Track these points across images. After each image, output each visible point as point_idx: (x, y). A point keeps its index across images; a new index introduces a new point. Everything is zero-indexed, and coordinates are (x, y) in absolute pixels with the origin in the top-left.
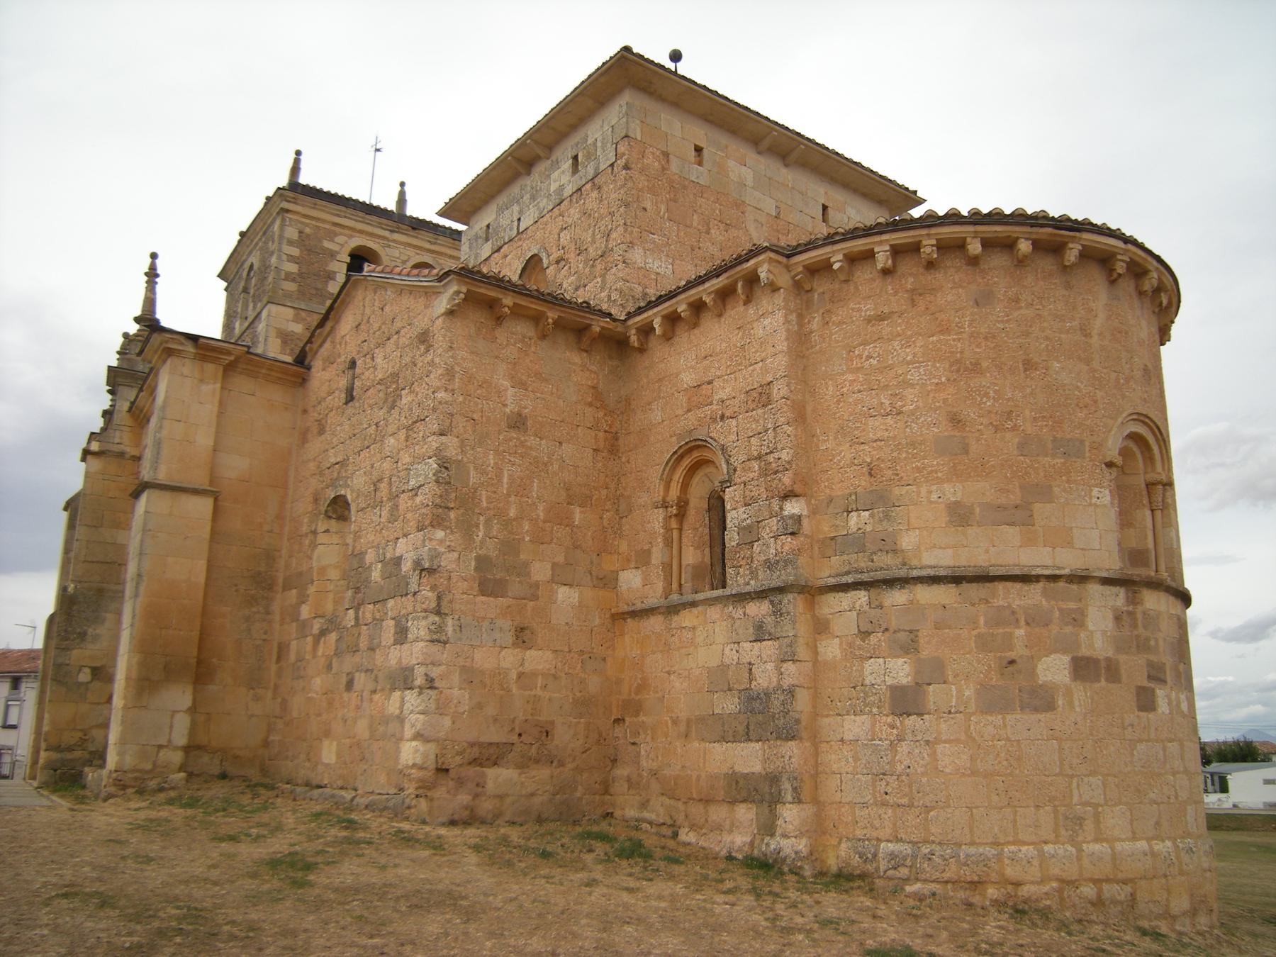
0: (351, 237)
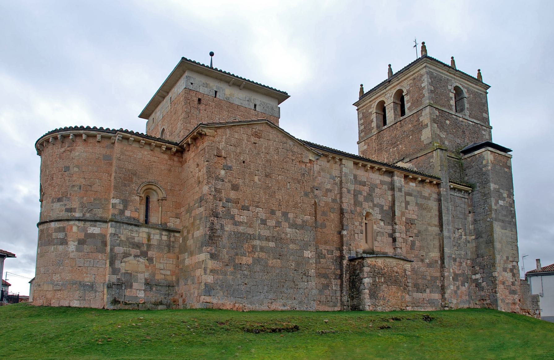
0: (375, 102)
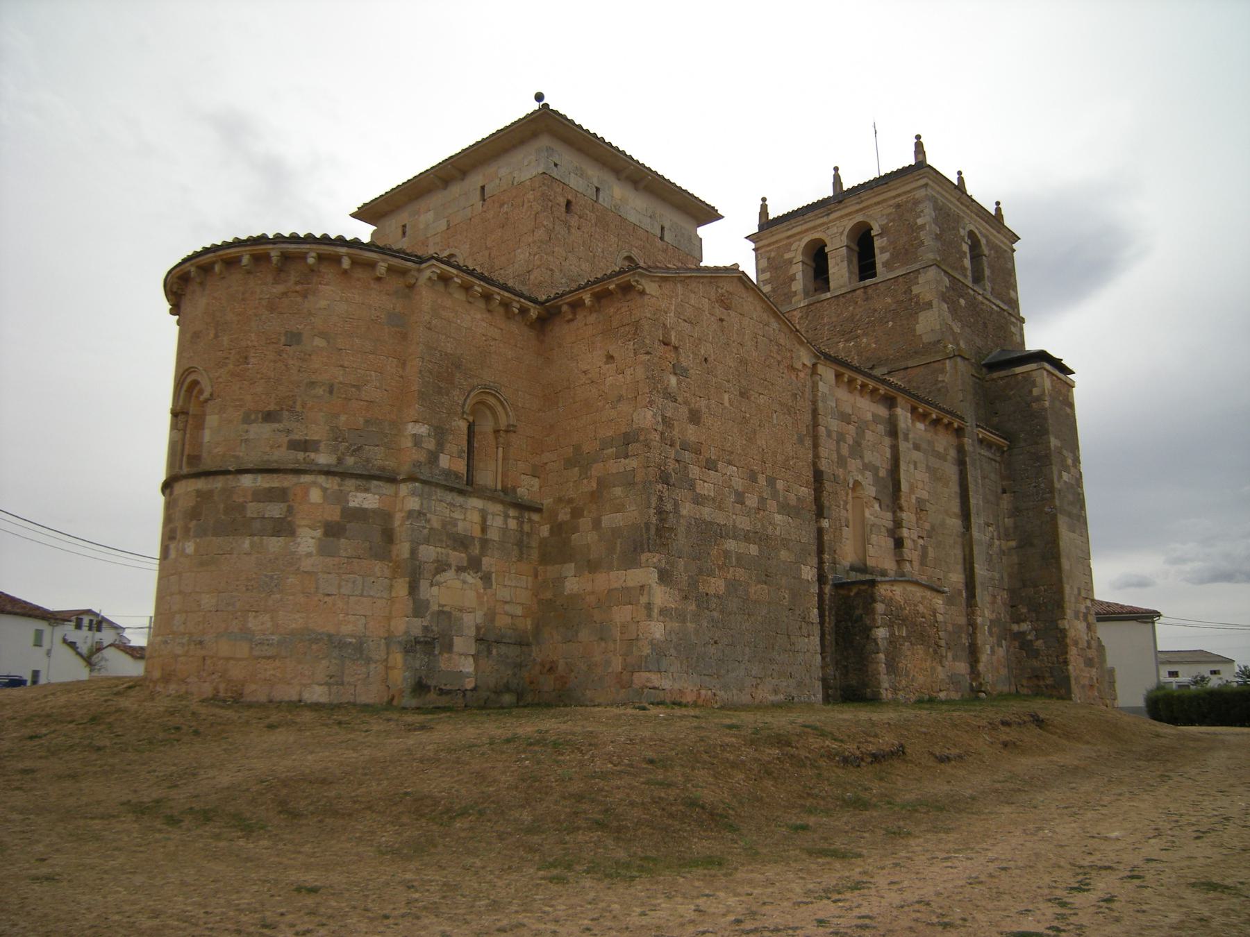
0: (800, 240)
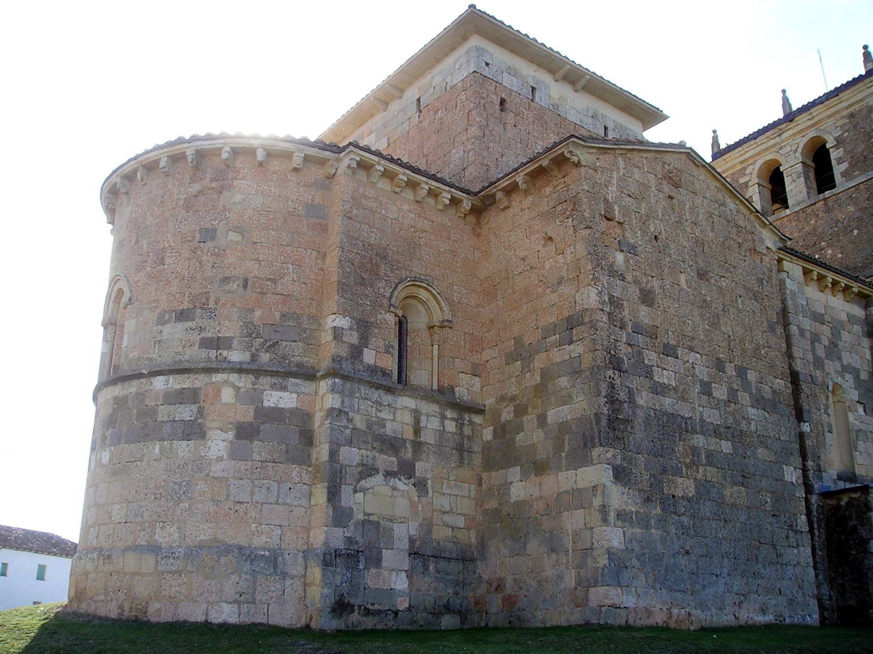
0: (754, 164)
